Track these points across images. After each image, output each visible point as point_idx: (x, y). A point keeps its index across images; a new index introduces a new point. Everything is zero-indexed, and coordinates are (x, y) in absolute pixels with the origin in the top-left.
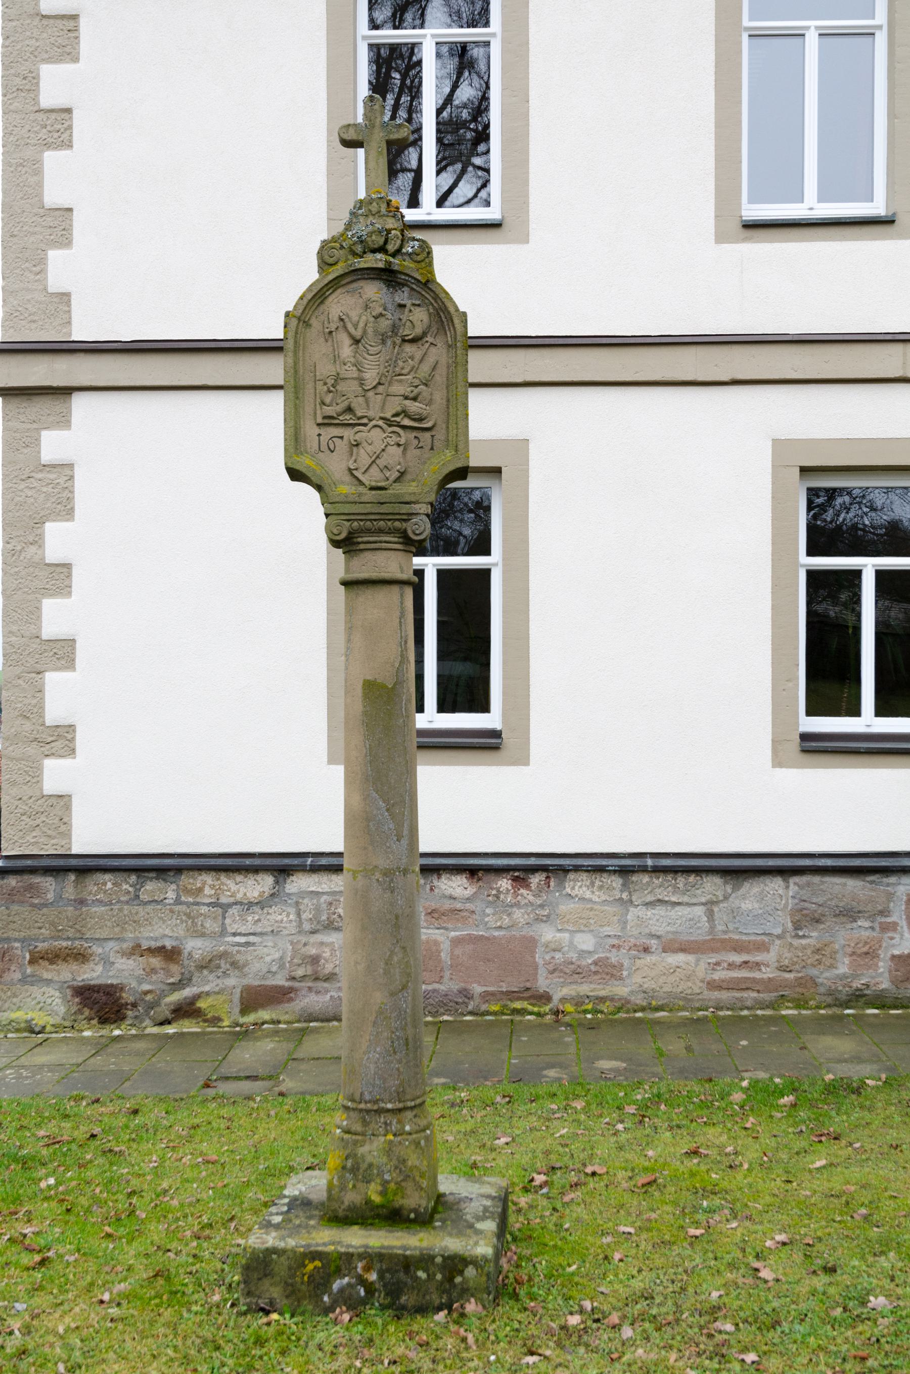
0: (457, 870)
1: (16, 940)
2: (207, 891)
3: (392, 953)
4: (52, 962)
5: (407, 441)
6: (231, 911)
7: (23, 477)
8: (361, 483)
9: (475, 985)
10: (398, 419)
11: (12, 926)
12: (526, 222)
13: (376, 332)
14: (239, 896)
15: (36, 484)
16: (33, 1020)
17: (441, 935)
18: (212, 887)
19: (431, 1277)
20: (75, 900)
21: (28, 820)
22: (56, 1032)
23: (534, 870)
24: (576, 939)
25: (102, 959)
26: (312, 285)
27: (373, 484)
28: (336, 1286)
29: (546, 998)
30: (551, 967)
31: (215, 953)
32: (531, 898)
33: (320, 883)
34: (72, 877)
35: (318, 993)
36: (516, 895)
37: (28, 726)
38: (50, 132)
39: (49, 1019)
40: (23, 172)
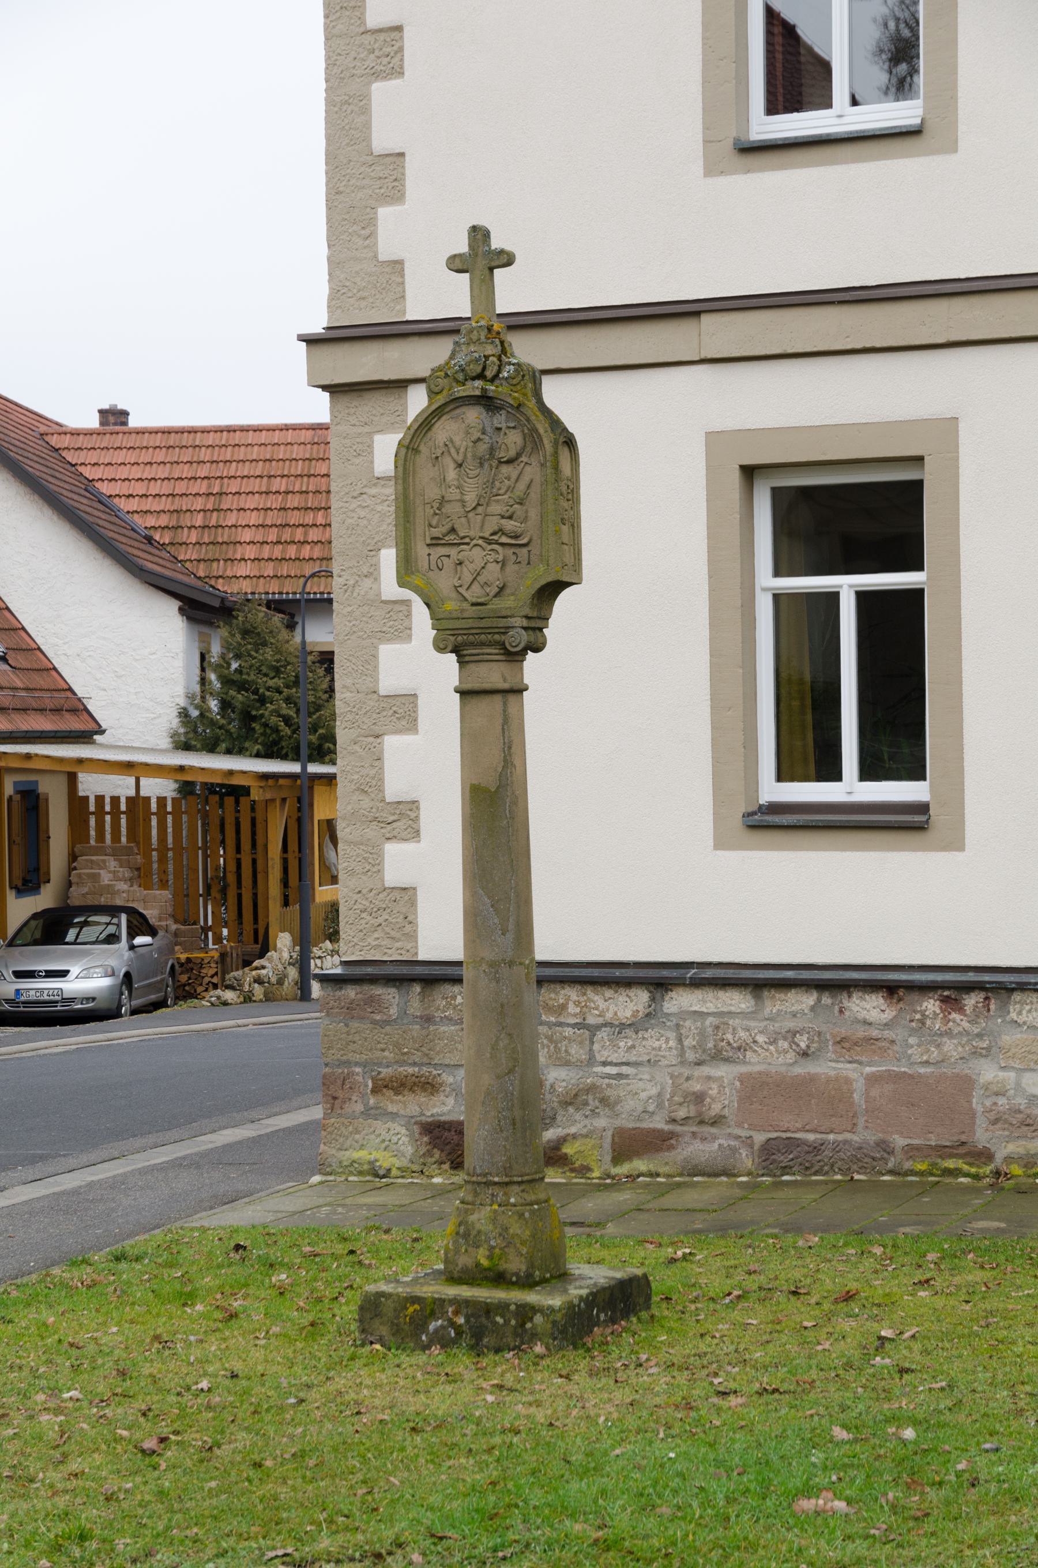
0: (871, 986)
1: (357, 1064)
2: (572, 1009)
3: (498, 1039)
4: (397, 1093)
5: (504, 557)
6: (599, 1035)
7: (355, 494)
8: (466, 600)
9: (896, 1136)
10: (495, 537)
11: (351, 1047)
12: (953, 125)
13: (474, 456)
14: (609, 1015)
15: (369, 502)
16: (377, 1161)
17: (854, 1070)
18: (577, 1003)
19: (507, 1322)
20: (421, 1017)
21: (369, 918)
22: (403, 1177)
23: (969, 988)
24: (1024, 1081)
25: (454, 1090)
26: (417, 416)
27: (474, 600)
28: (432, 1327)
29: (986, 1155)
30: (992, 1116)
31: (581, 1086)
32: (966, 1025)
33: (705, 1002)
34: (417, 988)
35: (704, 1139)
36: (946, 1020)
37: (366, 803)
38: (378, 57)
39: (394, 1160)
40: (349, 112)
